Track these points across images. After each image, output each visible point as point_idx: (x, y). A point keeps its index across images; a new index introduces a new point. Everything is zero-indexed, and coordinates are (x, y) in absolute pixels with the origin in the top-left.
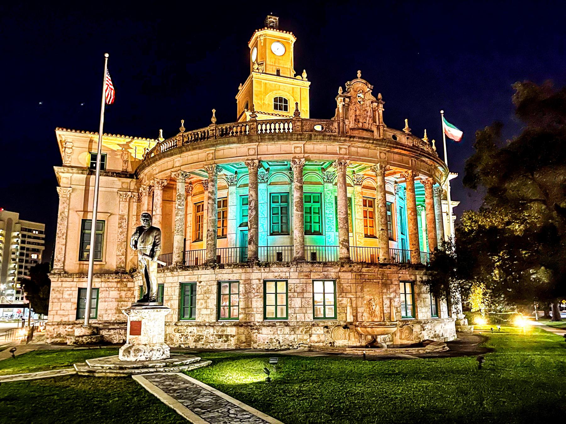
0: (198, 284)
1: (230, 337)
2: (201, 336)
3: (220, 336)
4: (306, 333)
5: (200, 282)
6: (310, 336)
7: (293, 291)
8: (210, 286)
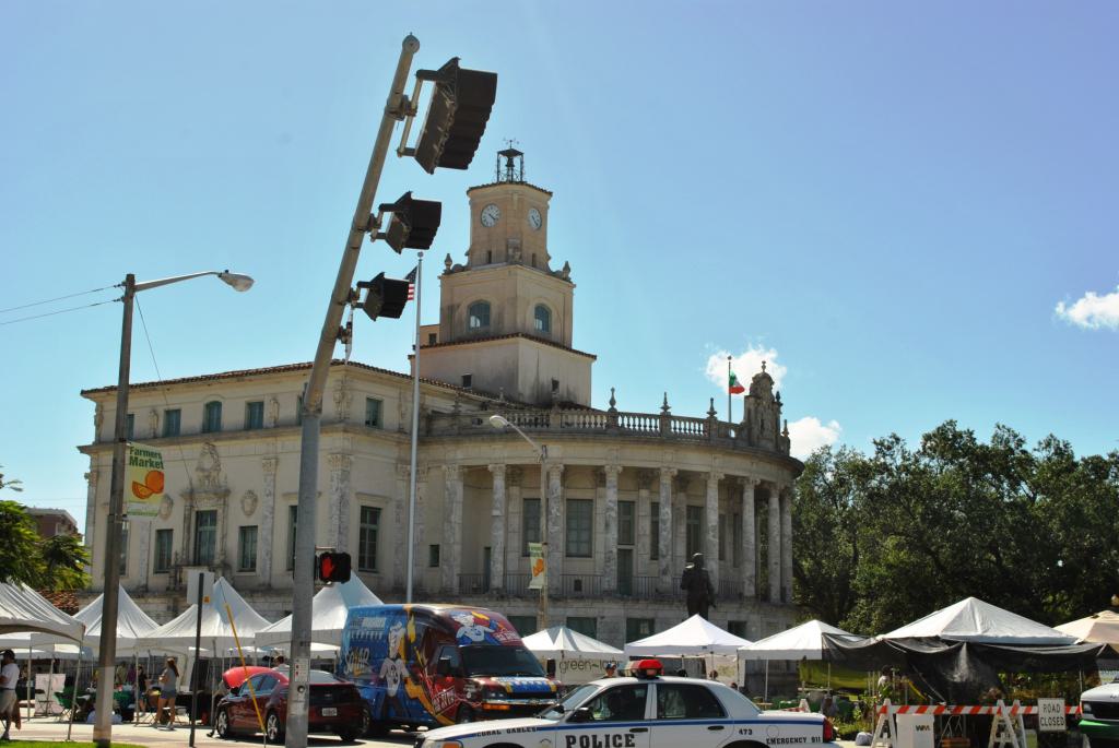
0: (599, 620)
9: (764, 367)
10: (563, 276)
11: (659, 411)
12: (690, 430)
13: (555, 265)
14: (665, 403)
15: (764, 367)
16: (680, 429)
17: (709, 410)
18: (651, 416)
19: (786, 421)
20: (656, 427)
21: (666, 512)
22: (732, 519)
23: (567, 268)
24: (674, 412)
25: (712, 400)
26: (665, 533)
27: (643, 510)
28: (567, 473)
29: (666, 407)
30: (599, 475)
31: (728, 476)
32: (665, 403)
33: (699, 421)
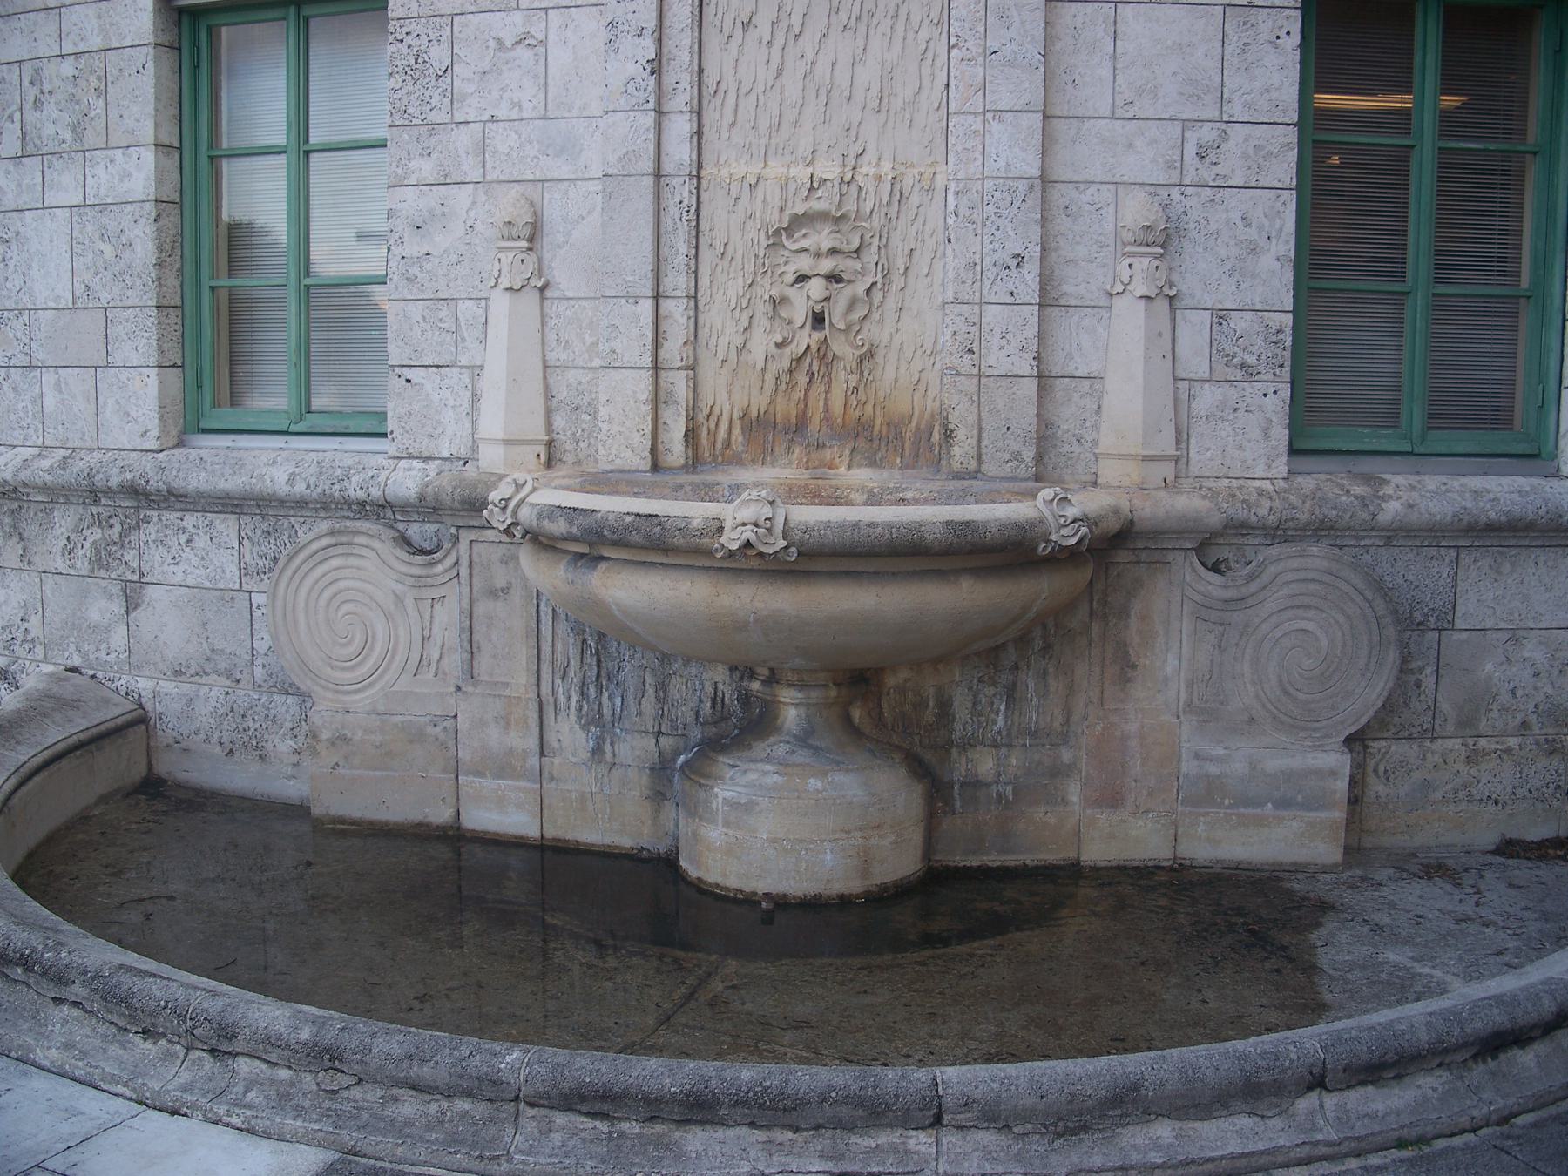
4: (102, 559)
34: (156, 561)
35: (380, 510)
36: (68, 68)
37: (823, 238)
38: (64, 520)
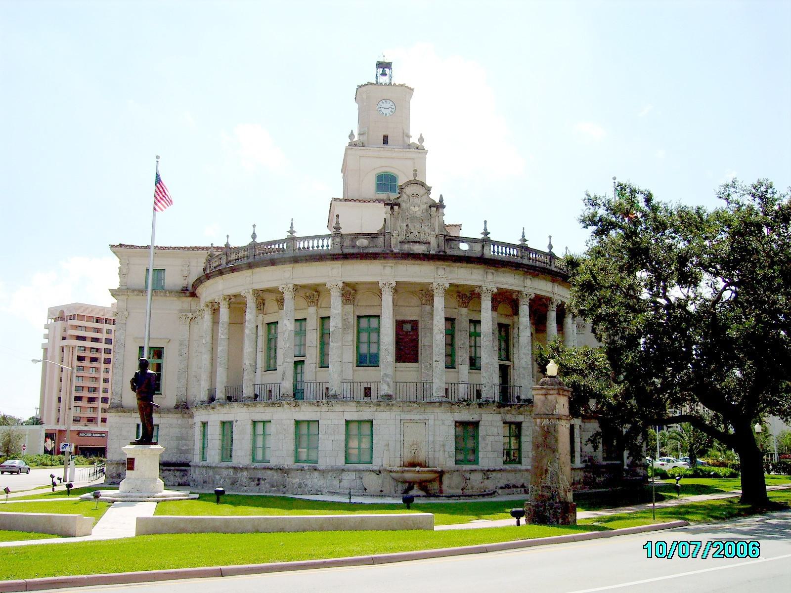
0: (234, 423)
1: (261, 481)
2: (236, 478)
3: (253, 479)
5: (236, 421)
6: (340, 482)
7: (324, 432)
8: (244, 425)
9: (415, 175)
10: (419, 148)
11: (481, 237)
12: (498, 253)
13: (414, 140)
14: (292, 227)
15: (415, 175)
16: (498, 253)
17: (483, 231)
18: (323, 237)
19: (338, 216)
20: (328, 246)
21: (335, 324)
22: (505, 333)
23: (421, 139)
24: (493, 237)
25: (485, 222)
26: (487, 343)
27: (313, 324)
28: (399, 288)
29: (486, 233)
30: (425, 294)
31: (537, 296)
32: (292, 227)
33: (513, 246)
34: (344, 477)
35: (373, 471)
36: (333, 426)
37: (415, 446)
38: (330, 474)
